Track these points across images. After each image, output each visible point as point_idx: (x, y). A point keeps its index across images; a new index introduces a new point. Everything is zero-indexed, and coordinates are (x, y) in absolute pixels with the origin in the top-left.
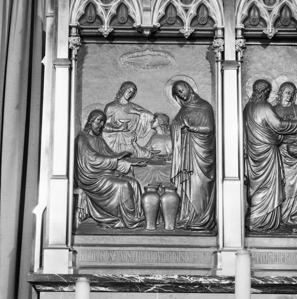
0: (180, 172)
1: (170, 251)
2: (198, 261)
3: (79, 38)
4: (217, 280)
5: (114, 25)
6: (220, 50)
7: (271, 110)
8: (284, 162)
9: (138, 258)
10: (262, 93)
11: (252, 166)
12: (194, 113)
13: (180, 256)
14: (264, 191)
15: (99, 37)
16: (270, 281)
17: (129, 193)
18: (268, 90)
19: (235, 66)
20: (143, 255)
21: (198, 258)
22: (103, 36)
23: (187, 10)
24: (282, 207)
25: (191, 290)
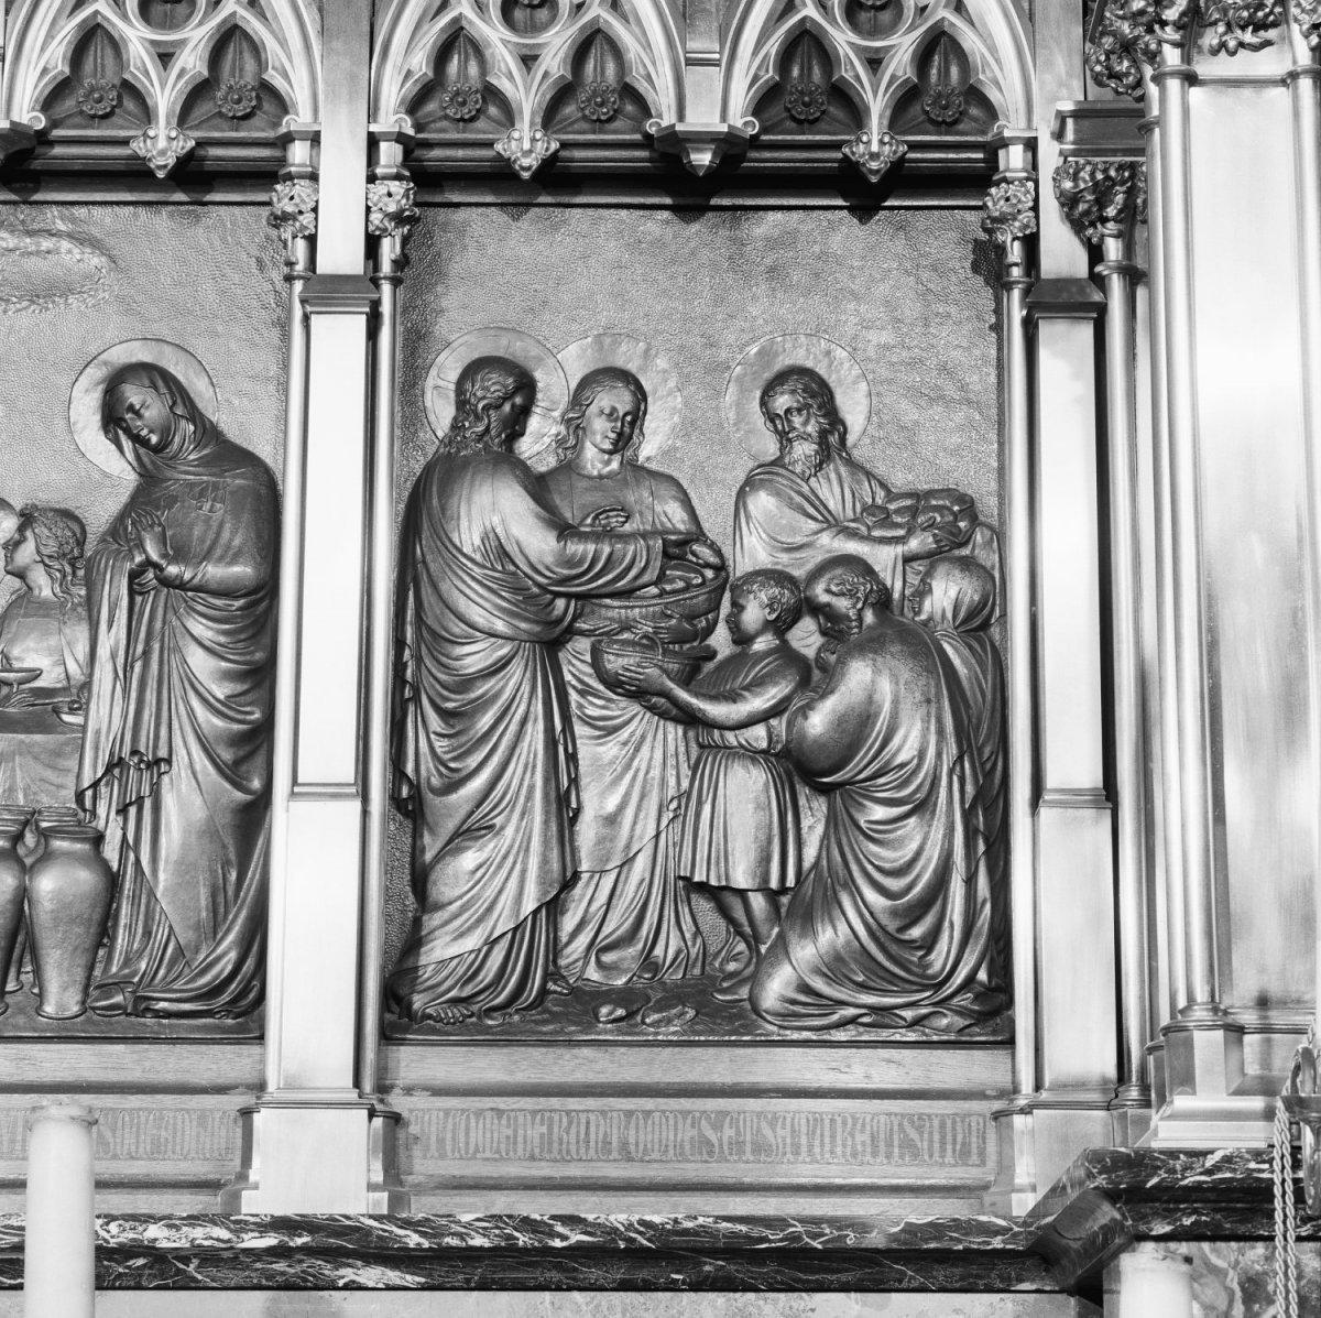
0: (115, 765)
3: (412, 185)
4: (224, 1234)
5: (197, 127)
6: (301, 231)
7: (521, 489)
8: (579, 717)
10: (488, 416)
11: (435, 733)
12: (186, 504)
15: (498, 178)
16: (453, 1234)
18: (518, 400)
19: (364, 299)
22: (150, 174)
23: (874, 62)
24: (563, 913)
25: (114, 1280)
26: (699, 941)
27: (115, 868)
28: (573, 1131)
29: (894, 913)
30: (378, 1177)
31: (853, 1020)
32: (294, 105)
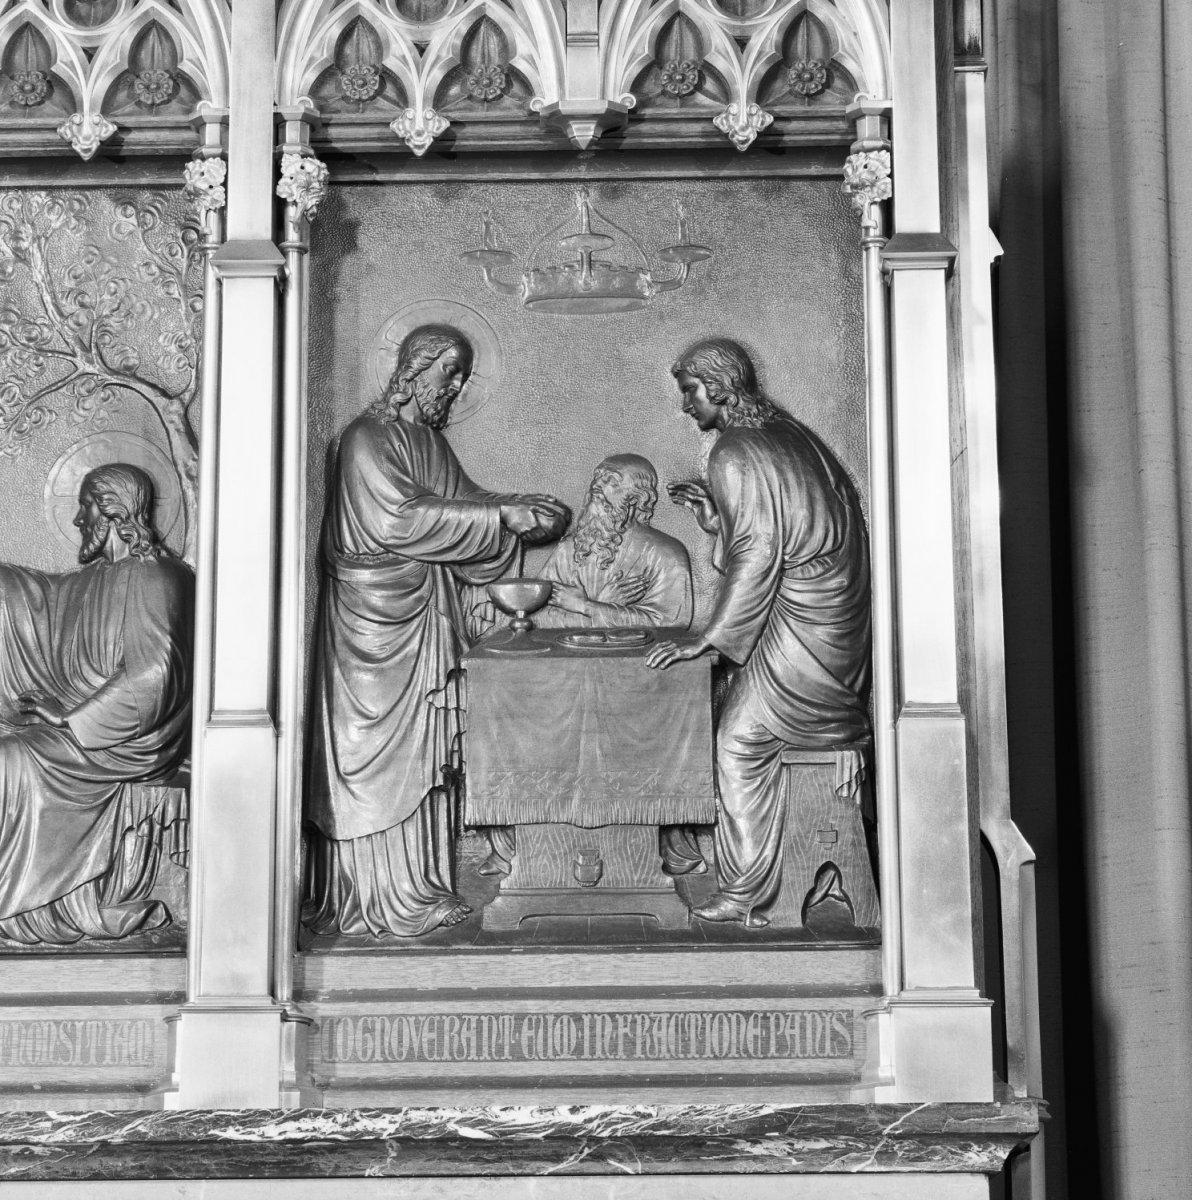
30: (290, 1075)
32: (207, 92)
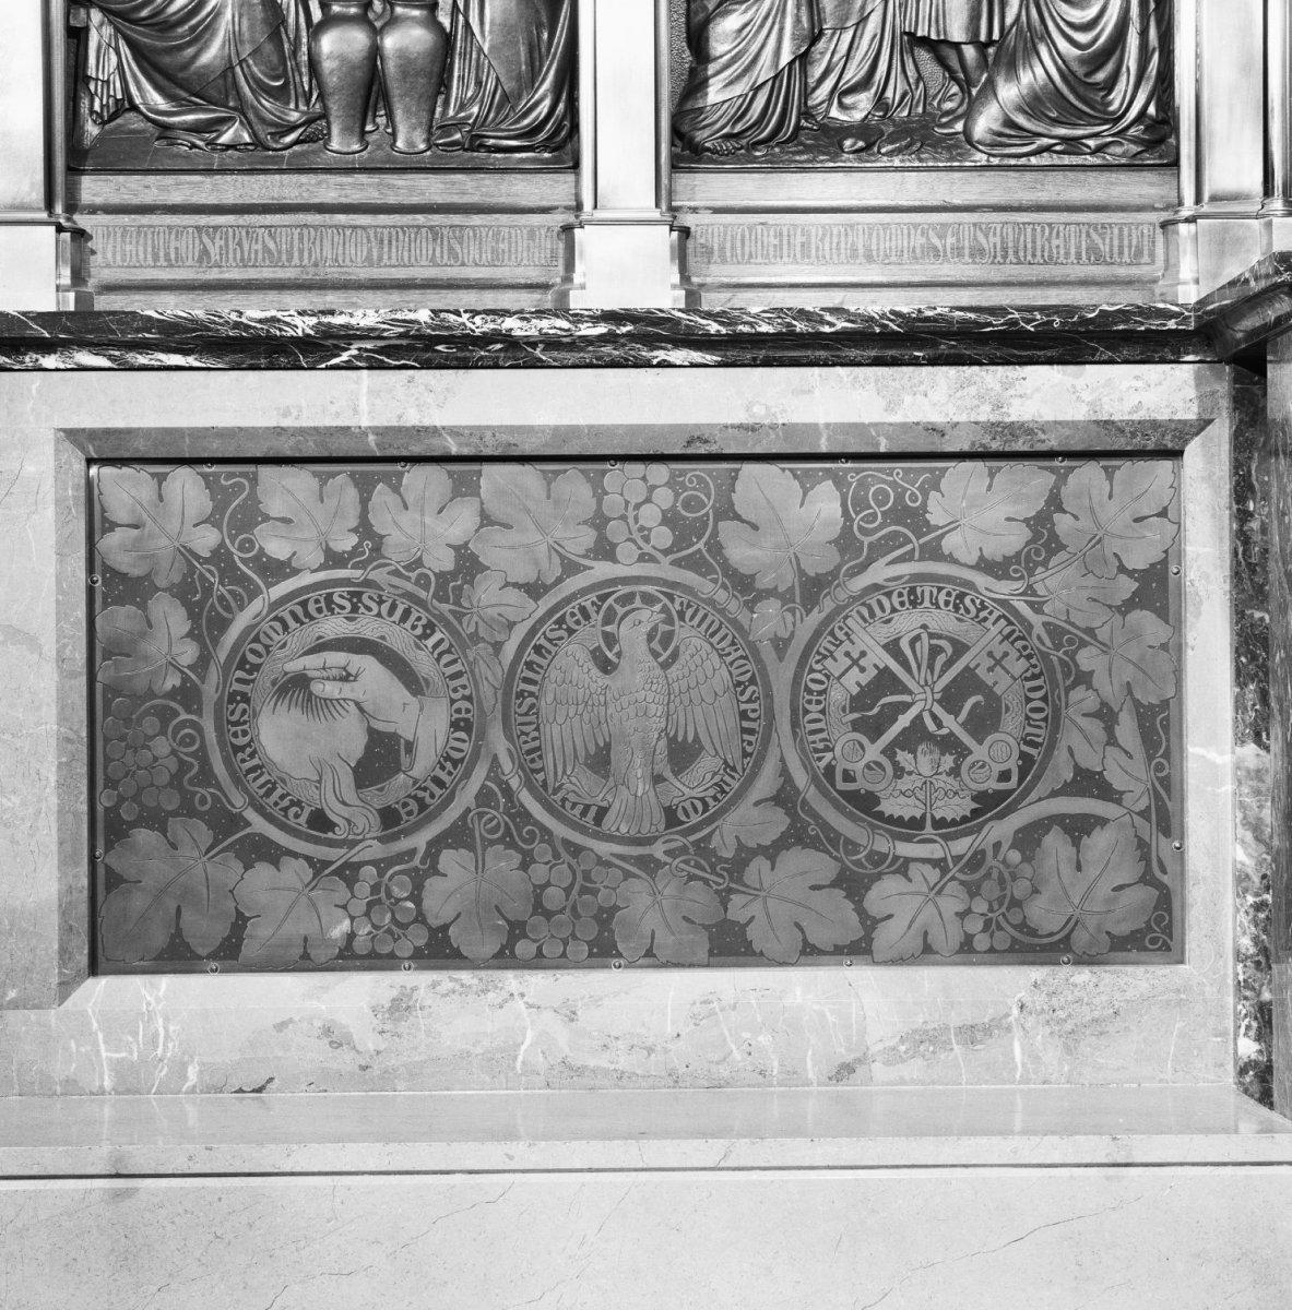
1: (413, 226)
2: (510, 259)
4: (565, 324)
9: (301, 252)
13: (445, 243)
14: (744, 7)
16: (745, 323)
17: (265, 21)
20: (318, 242)
21: (510, 248)
24: (811, 63)
26: (921, 85)
27: (448, 30)
28: (827, 239)
29: (1082, 61)
30: (66, 280)
31: (1048, 149)
